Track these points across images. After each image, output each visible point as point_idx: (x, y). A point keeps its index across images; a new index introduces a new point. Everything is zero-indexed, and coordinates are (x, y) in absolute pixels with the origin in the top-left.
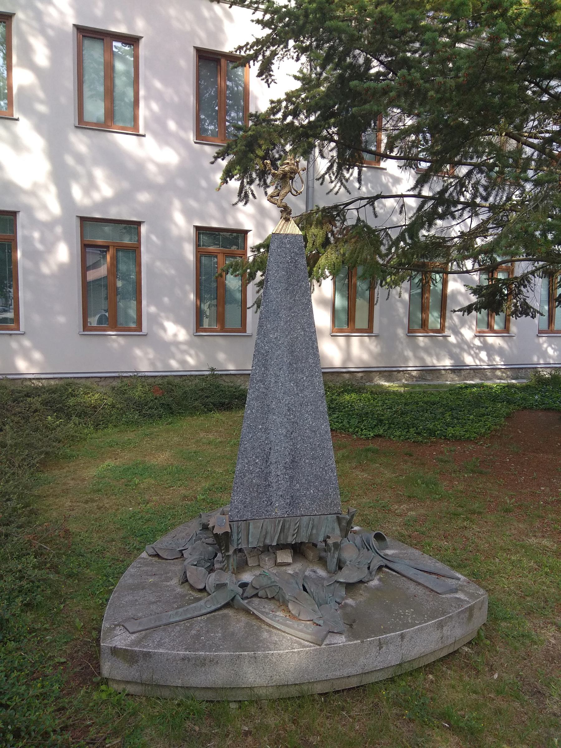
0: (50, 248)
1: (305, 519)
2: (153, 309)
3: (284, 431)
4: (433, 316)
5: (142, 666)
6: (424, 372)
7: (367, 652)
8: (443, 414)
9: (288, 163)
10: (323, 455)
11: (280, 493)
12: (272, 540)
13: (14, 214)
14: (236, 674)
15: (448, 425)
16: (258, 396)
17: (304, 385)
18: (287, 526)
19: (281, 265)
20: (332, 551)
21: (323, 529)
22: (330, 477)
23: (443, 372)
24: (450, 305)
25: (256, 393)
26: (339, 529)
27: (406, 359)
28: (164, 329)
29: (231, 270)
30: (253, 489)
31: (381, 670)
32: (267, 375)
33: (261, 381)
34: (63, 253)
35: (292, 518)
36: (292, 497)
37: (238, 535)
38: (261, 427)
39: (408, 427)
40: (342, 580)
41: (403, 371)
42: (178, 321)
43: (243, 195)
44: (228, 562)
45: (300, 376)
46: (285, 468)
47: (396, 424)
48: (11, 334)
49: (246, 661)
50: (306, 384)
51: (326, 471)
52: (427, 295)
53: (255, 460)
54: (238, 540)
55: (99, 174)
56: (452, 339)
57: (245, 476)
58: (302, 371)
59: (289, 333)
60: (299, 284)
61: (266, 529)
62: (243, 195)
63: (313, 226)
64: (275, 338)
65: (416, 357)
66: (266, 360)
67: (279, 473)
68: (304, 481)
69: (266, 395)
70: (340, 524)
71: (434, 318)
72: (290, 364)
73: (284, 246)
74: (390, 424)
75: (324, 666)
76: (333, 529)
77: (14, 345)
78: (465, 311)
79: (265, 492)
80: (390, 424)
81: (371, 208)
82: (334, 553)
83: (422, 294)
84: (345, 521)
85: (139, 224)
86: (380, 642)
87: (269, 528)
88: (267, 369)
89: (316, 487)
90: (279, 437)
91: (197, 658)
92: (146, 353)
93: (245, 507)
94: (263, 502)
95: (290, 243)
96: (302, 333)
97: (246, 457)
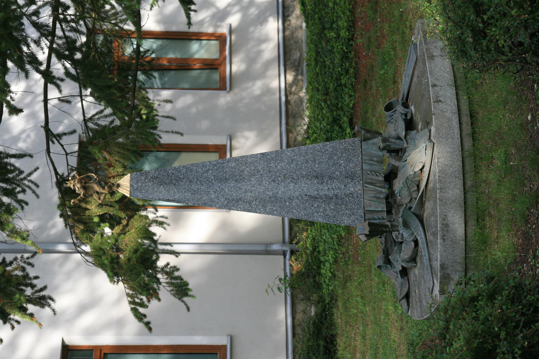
1: (365, 167)
3: (292, 185)
4: (198, 51)
5: (452, 270)
6: (288, 63)
7: (442, 111)
8: (328, 41)
9: (74, 185)
10: (311, 154)
11: (343, 187)
12: (381, 193)
14: (454, 202)
15: (338, 36)
16: (262, 206)
18: (370, 180)
21: (373, 152)
22: (330, 147)
23: (287, 33)
24: (180, 26)
26: (373, 140)
27: (267, 91)
29: (141, 310)
30: (339, 208)
31: (458, 99)
32: (245, 199)
35: (364, 177)
36: (346, 177)
38: (288, 203)
39: (341, 85)
40: (404, 133)
41: (286, 96)
45: (246, 173)
46: (322, 183)
47: (337, 102)
49: (443, 195)
50: (253, 168)
51: (325, 151)
52: (165, 63)
53: (315, 207)
54: (380, 219)
56: (234, 20)
57: (328, 215)
58: (243, 171)
59: (210, 182)
60: (171, 175)
61: (372, 197)
63: (88, 207)
64: (215, 193)
65: (262, 75)
69: (261, 199)
71: (200, 51)
74: (338, 108)
75: (449, 141)
76: (373, 144)
78: (190, 9)
79: (342, 199)
80: (338, 108)
81: (64, 137)
82: (392, 142)
83: (162, 69)
86: (436, 102)
87: (372, 195)
88: (240, 199)
89: (338, 159)
90: (296, 189)
91: (442, 230)
93: (353, 214)
96: (211, 172)
97: (313, 214)
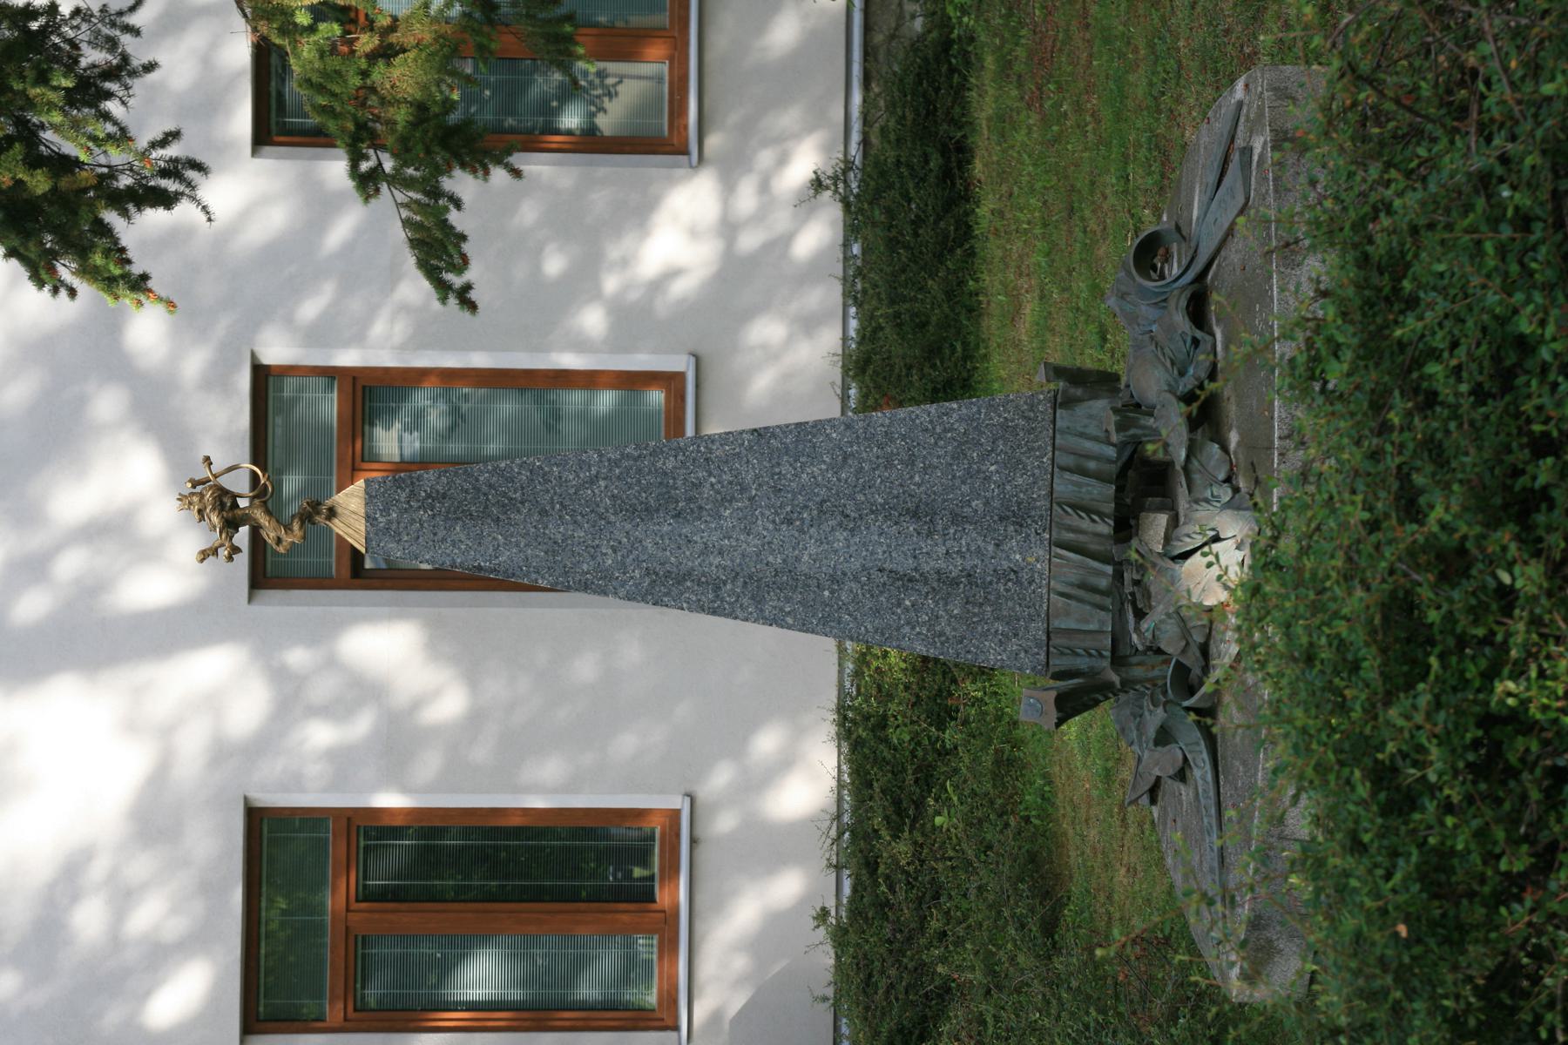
0: (363, 690)
2: (593, 320)
3: (841, 535)
10: (903, 438)
11: (991, 548)
13: (256, 817)
16: (753, 598)
17: (731, 483)
19: (441, 534)
20: (1139, 432)
22: (961, 419)
25: (745, 601)
28: (672, 274)
30: (975, 615)
32: (704, 575)
33: (717, 589)
34: (386, 643)
36: (1001, 519)
37: (1078, 655)
38: (826, 593)
42: (640, 213)
43: (171, 185)
44: (1140, 682)
45: (707, 491)
46: (930, 534)
48: (694, 841)
50: (726, 477)
51: (945, 431)
55: (74, 500)
57: (942, 634)
58: (697, 485)
62: (171, 185)
64: (615, 551)
66: (668, 574)
67: (941, 550)
68: (965, 488)
69: (751, 577)
70: (1080, 400)
72: (678, 515)
73: (394, 526)
77: (724, 823)
84: (1072, 391)
85: (262, 376)
89: (983, 458)
90: (853, 549)
92: (771, 354)
93: (1016, 635)
94: (1007, 591)
95: (386, 511)
96: (602, 483)
97: (898, 629)
